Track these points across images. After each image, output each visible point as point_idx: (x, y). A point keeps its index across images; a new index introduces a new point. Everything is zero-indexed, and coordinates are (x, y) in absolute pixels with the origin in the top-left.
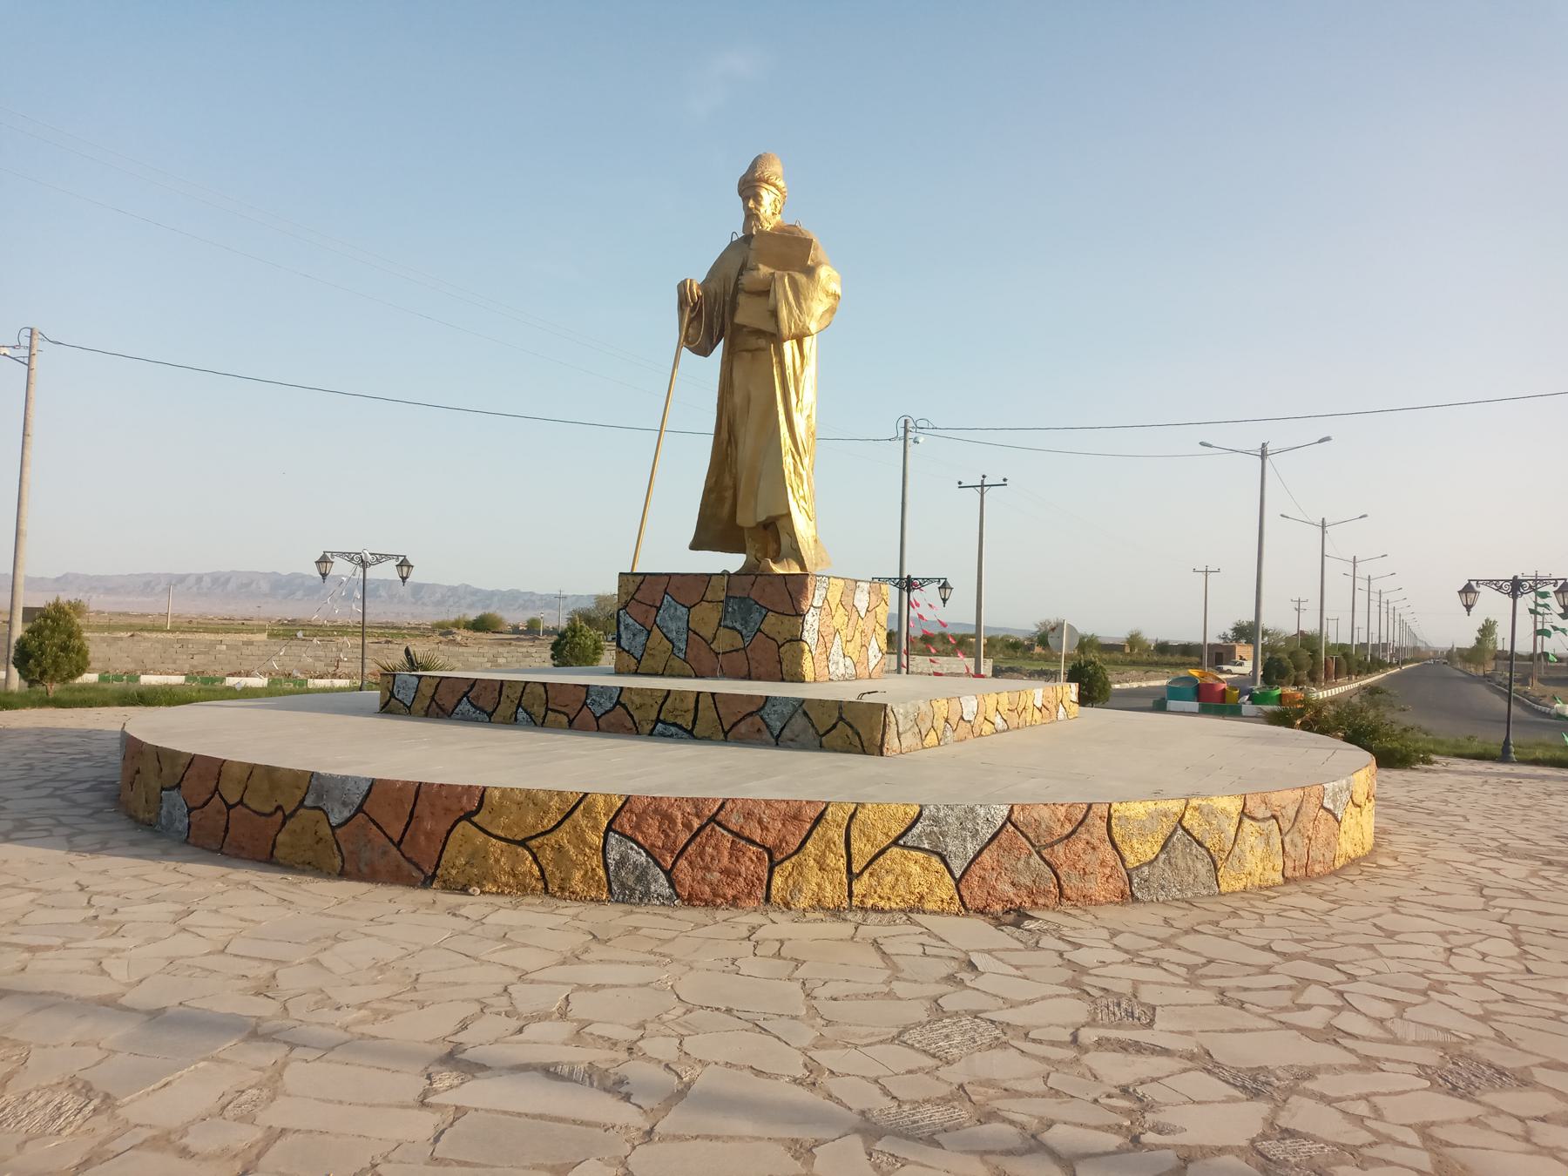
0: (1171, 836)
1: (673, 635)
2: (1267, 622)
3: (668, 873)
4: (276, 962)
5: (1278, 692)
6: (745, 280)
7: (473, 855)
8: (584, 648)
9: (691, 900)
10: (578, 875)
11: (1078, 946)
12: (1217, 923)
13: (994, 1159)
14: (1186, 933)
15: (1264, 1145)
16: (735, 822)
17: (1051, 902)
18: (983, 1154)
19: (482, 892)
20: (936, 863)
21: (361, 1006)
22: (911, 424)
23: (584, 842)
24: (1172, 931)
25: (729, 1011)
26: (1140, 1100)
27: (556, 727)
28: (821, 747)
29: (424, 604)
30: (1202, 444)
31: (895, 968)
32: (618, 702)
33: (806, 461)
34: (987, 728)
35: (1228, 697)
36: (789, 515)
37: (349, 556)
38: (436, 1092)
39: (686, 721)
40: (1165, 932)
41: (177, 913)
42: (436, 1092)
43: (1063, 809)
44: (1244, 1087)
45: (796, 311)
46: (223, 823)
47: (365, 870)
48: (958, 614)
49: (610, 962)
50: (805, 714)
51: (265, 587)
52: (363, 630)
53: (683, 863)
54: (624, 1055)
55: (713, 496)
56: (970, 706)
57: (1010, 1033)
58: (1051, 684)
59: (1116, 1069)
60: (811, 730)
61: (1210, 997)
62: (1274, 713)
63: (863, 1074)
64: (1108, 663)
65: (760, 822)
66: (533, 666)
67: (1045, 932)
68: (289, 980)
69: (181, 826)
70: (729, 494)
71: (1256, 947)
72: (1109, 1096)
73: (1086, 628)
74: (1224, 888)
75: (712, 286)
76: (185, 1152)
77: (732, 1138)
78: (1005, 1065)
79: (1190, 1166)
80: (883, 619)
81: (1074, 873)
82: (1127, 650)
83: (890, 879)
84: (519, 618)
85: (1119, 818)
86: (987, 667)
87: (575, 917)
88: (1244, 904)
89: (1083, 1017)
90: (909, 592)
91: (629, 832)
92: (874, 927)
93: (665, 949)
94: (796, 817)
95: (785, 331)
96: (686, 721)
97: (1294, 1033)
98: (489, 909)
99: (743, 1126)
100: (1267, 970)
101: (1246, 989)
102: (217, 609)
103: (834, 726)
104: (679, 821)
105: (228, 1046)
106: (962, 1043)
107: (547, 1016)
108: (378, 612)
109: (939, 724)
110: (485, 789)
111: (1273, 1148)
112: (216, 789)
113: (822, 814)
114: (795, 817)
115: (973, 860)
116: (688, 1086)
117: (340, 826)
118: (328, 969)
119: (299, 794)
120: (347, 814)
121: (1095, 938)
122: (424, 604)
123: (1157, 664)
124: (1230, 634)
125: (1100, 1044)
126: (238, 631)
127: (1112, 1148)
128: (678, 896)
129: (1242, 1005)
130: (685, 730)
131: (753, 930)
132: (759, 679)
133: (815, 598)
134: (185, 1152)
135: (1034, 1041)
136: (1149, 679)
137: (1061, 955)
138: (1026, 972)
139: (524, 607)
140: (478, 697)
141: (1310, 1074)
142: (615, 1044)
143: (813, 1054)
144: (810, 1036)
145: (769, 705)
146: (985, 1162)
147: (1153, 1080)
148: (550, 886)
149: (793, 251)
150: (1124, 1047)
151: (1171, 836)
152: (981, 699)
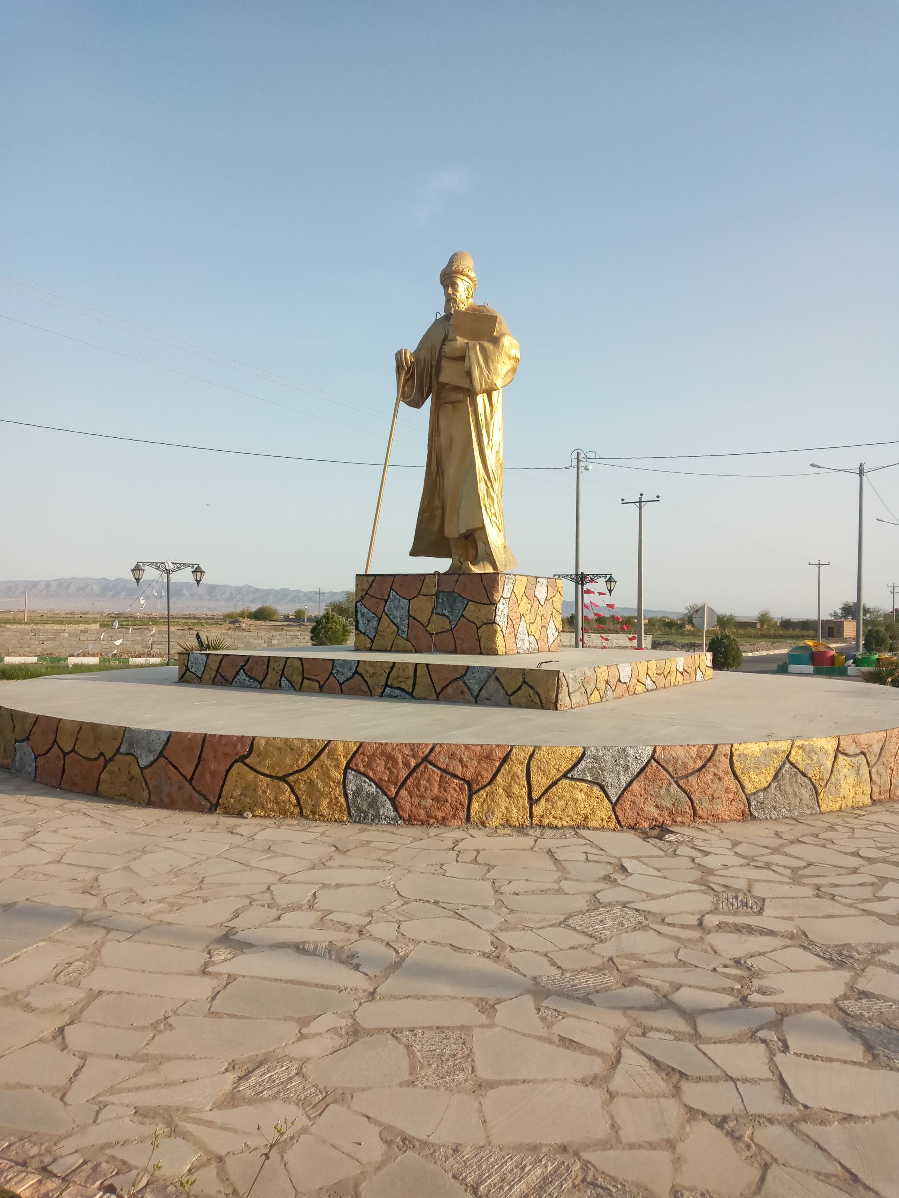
0: (780, 769)
1: (397, 621)
2: (868, 601)
3: (393, 800)
4: (97, 868)
5: (876, 657)
6: (446, 349)
7: (246, 788)
8: (335, 632)
9: (410, 821)
10: (325, 802)
11: (706, 853)
12: (817, 836)
13: (634, 1014)
14: (792, 842)
15: (845, 1004)
16: (442, 761)
17: (687, 820)
18: (625, 1009)
19: (253, 816)
20: (597, 791)
21: (160, 901)
22: (582, 456)
23: (329, 777)
24: (781, 841)
25: (436, 903)
26: (749, 969)
27: (310, 691)
28: (510, 705)
29: (218, 600)
30: (812, 465)
31: (564, 870)
32: (356, 672)
33: (496, 486)
34: (640, 688)
35: (836, 661)
36: (484, 528)
37: (156, 565)
38: (214, 963)
39: (408, 686)
40: (776, 842)
41: (26, 833)
42: (214, 963)
43: (695, 749)
44: (831, 960)
45: (486, 372)
46: (61, 765)
47: (166, 800)
48: (623, 600)
49: (348, 867)
50: (497, 678)
51: (97, 588)
52: (168, 620)
53: (403, 793)
54: (355, 936)
55: (426, 514)
56: (625, 672)
57: (650, 919)
58: (690, 654)
59: (731, 946)
60: (502, 692)
61: (809, 891)
62: (870, 673)
63: (536, 949)
64: (740, 636)
65: (461, 761)
66: (298, 646)
67: (680, 842)
68: (107, 882)
69: (31, 769)
70: (438, 513)
71: (846, 853)
72: (725, 966)
73: (724, 609)
74: (823, 808)
75: (422, 355)
76: (28, 1008)
77: (434, 997)
78: (645, 943)
79: (785, 1019)
80: (558, 606)
81: (705, 798)
82: (759, 626)
83: (561, 803)
84: (287, 609)
85: (739, 756)
86: (647, 641)
87: (323, 834)
88: (839, 821)
89: (708, 907)
90: (582, 585)
91: (362, 770)
92: (549, 840)
93: (389, 858)
94: (489, 757)
95: (478, 387)
96: (408, 686)
97: (873, 918)
98: (258, 829)
99: (443, 989)
100: (854, 871)
101: (837, 885)
102: (61, 606)
103: (520, 688)
104: (400, 761)
105: (61, 930)
106: (613, 926)
107: (299, 908)
108: (180, 607)
109: (602, 685)
110: (254, 738)
111: (852, 1006)
112: (55, 741)
113: (508, 754)
114: (488, 757)
115: (626, 789)
116: (403, 959)
117: (146, 767)
118: (137, 874)
119: (116, 744)
120: (151, 758)
121: (720, 848)
122: (218, 600)
123: (781, 637)
124: (839, 612)
125: (720, 927)
126: (78, 623)
127: (725, 1005)
128: (401, 817)
129: (833, 898)
130: (407, 693)
131: (457, 842)
132: (463, 653)
133: (505, 590)
134: (28, 1008)
135: (669, 925)
136: (774, 649)
137: (693, 860)
138: (665, 873)
139: (293, 601)
140: (251, 670)
141: (884, 950)
142: (349, 928)
143: (500, 935)
144: (497, 921)
145: (470, 672)
146: (626, 1016)
147: (760, 954)
148: (305, 811)
149: (483, 326)
150: (739, 929)
151: (780, 769)
152: (631, 664)
